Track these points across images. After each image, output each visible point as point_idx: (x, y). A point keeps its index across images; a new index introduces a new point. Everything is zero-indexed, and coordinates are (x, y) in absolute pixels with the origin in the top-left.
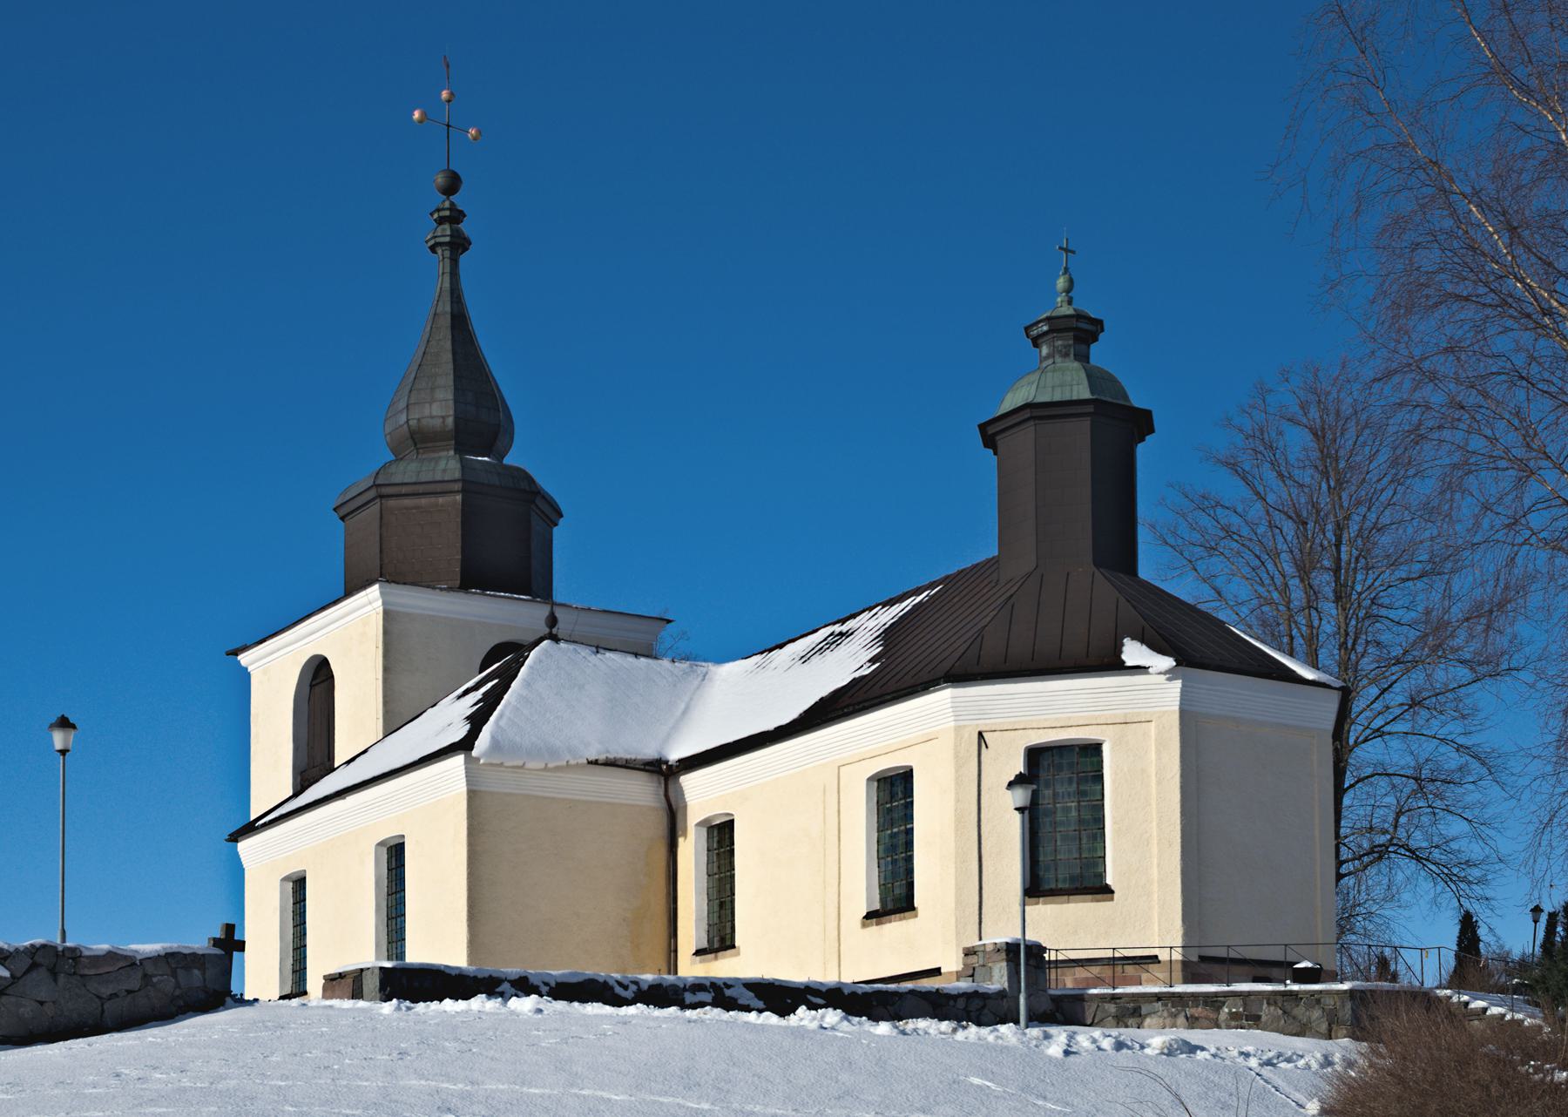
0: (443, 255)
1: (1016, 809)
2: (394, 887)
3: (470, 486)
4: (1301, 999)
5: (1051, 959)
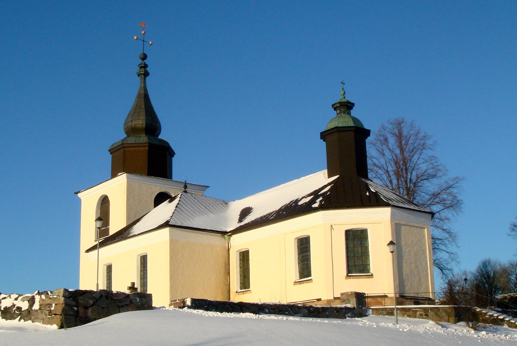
0: (142, 77)
1: (391, 252)
2: (143, 269)
3: (151, 146)
4: (440, 309)
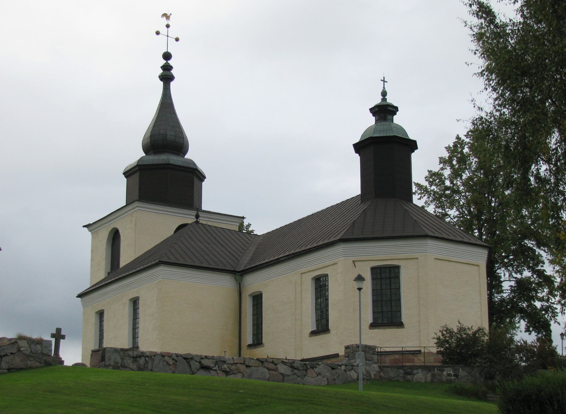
5: (378, 351)
